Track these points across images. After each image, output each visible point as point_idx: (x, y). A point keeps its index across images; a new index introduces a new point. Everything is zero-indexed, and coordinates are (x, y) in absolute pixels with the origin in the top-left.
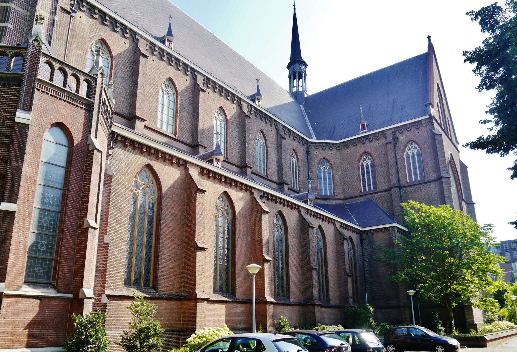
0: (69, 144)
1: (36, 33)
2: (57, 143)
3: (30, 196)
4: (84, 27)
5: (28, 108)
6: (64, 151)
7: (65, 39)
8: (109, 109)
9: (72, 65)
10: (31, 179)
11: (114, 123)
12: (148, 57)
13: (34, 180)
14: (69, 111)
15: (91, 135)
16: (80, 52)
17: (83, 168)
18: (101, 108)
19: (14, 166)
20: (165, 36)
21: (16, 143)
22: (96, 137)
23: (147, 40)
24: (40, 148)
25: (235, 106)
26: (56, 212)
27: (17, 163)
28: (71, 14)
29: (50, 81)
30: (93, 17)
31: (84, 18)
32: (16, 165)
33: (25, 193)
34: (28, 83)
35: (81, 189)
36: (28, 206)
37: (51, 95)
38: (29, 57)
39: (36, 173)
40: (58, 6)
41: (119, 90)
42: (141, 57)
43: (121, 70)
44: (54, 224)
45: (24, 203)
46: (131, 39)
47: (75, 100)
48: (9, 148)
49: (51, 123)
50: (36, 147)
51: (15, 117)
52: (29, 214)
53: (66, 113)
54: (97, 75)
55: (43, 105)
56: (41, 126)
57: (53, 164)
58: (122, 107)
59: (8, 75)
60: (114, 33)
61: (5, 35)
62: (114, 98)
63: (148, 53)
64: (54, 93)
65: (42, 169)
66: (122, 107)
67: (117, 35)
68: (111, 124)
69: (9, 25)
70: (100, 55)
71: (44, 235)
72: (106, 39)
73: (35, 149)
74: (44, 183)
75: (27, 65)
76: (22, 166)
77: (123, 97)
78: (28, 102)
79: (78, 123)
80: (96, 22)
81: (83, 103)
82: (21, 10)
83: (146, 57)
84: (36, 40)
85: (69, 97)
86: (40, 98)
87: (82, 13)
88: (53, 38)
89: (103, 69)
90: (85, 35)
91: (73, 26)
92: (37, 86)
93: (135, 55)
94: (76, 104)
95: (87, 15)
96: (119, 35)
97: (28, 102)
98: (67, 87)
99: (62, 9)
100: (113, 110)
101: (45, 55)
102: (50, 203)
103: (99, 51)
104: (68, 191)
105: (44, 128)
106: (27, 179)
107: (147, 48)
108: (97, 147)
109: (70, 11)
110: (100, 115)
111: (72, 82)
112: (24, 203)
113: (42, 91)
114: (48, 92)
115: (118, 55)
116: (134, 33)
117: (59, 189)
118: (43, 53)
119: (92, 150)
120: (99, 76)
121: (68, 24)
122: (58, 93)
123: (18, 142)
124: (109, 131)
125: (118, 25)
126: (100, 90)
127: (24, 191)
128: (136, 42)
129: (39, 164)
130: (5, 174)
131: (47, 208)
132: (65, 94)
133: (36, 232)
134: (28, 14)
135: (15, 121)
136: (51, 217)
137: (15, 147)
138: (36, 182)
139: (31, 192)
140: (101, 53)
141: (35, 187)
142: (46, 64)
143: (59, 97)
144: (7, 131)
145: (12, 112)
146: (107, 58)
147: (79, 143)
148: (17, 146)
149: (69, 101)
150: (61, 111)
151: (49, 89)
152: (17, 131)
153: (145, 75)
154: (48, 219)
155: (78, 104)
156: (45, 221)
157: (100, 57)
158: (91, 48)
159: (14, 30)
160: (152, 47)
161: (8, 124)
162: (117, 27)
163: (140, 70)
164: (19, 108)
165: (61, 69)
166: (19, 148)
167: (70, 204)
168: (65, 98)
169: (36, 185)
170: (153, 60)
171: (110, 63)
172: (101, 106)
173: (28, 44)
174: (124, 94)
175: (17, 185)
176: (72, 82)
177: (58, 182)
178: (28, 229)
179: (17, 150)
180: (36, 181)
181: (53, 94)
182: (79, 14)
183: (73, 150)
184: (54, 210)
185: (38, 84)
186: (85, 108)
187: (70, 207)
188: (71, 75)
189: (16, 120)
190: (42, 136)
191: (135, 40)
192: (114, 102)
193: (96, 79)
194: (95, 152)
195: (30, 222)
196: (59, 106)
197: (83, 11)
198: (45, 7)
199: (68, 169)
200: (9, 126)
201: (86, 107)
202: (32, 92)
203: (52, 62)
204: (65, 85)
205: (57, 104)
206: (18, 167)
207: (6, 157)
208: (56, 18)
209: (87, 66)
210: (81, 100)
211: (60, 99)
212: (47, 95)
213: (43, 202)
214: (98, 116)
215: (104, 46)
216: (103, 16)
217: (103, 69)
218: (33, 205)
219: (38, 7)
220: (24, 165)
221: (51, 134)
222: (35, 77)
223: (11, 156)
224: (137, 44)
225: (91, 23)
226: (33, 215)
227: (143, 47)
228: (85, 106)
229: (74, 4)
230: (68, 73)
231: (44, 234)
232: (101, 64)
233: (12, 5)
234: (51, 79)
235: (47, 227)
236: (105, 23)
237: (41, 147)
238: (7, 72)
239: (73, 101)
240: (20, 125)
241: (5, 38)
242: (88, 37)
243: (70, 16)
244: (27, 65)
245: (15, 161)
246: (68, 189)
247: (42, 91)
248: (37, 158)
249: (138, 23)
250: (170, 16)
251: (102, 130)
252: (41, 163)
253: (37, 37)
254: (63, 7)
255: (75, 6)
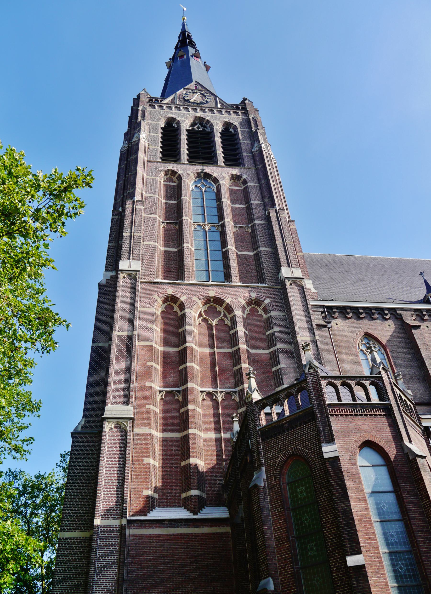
0: (386, 462)
1: (308, 361)
2: (373, 466)
3: (372, 540)
4: (344, 332)
5: (331, 440)
6: (383, 471)
7: (332, 352)
8: (409, 403)
9: (349, 374)
10: (365, 518)
11: (423, 417)
12: (420, 326)
13: (369, 518)
14: (371, 424)
15: (404, 441)
16: (351, 358)
17: (414, 485)
18: (400, 406)
19: (343, 509)
20: (426, 295)
21: (335, 482)
22: (410, 441)
23: (410, 310)
24: (359, 478)
25: (390, 322)
26: (407, 552)
27: (344, 504)
28: (328, 326)
29: (338, 401)
30: (348, 318)
31: (340, 323)
32: (344, 507)
33: (365, 538)
34: (321, 412)
35: (423, 512)
36: (375, 553)
37: (346, 415)
38: (311, 387)
39: (366, 509)
40: (314, 326)
41: (408, 377)
42: (413, 331)
43: (399, 355)
44: (413, 570)
45: (369, 551)
46: (394, 318)
47: (371, 409)
48: (330, 490)
49: (358, 445)
50: (355, 478)
51: (322, 453)
52: (380, 563)
53: (368, 428)
54: (380, 373)
55: (343, 430)
56: (351, 453)
57: (380, 492)
58: (420, 394)
59: (301, 414)
60: (374, 321)
61: (282, 377)
62: (408, 389)
63: (417, 322)
64: (347, 412)
65: (370, 501)
66: (420, 394)
67: (378, 321)
68: (419, 419)
69: (283, 366)
70: (373, 350)
71: (407, 588)
72: (370, 332)
73: (355, 482)
74: (380, 518)
75: (313, 395)
76: (350, 505)
77: (416, 382)
78: (328, 432)
79: (385, 433)
80: (353, 320)
81: (380, 409)
82: (286, 347)
83: (418, 327)
84: (311, 368)
85: (363, 409)
86: (338, 423)
87: (336, 320)
88: (322, 357)
89: (383, 363)
90: (348, 339)
91: (334, 336)
92: (330, 412)
93: (406, 332)
94: (373, 413)
95: (341, 319)
96: (380, 320)
97: (328, 432)
98: (357, 399)
99: (318, 326)
100: (413, 402)
101: (324, 378)
102: (396, 542)
103: (371, 347)
104: (410, 520)
105: (354, 454)
106: (360, 520)
107: (414, 317)
108: (418, 453)
109: (326, 324)
110: (404, 415)
111: (360, 393)
112: (369, 551)
113: (336, 415)
114: (341, 413)
115: (389, 341)
116: (393, 311)
117: (398, 520)
118: (321, 377)
119: (413, 459)
120: (383, 372)
121: (329, 337)
122: (351, 409)
123: (336, 480)
124: (421, 429)
125: (374, 311)
126: (390, 387)
127: (363, 536)
128: (399, 318)
129: (365, 497)
130: (337, 521)
131: (396, 550)
132: (358, 408)
133: (397, 585)
134: (293, 347)
135: (325, 457)
136: (405, 560)
137: (336, 487)
138: (371, 521)
139: (371, 535)
140: (373, 349)
141: (373, 527)
142: (327, 386)
143: (353, 413)
144: (321, 472)
145: (318, 450)
146: (379, 350)
147: (395, 456)
148: (337, 484)
149: (366, 413)
150: (362, 428)
151: (342, 409)
152: (330, 467)
153: (427, 347)
154: (403, 564)
155: (376, 413)
156: (401, 568)
157: (374, 352)
158: (359, 348)
159: (287, 368)
160: (419, 313)
161: (319, 464)
162: (374, 314)
163: (419, 345)
164: (322, 443)
165: (343, 384)
166: (339, 486)
167: (419, 537)
168: (359, 412)
169: (372, 524)
170: (427, 327)
171: (384, 353)
172: (399, 404)
173: (305, 375)
174: (415, 378)
175: (354, 530)
176: (360, 393)
177: (395, 512)
178: (386, 584)
179: (338, 489)
180: (370, 518)
181: (347, 414)
182: (334, 322)
183: (393, 467)
184: (405, 549)
185: (329, 409)
186: (384, 413)
187: (421, 541)
188: (355, 385)
189: (326, 456)
190: (355, 464)
191: (397, 317)
192: (411, 393)
193: (381, 378)
194: (418, 459)
195: (384, 574)
196: (358, 423)
197: (336, 318)
198: (304, 333)
199: (398, 492)
200: (321, 465)
201: (385, 412)
202: (328, 420)
203: (333, 381)
204: (354, 399)
205: (356, 422)
206: (347, 508)
207: (331, 501)
208: (317, 338)
209: (363, 368)
210: (376, 407)
211: (356, 415)
212: (342, 418)
213: (388, 544)
214: (402, 416)
215: (371, 339)
216: (356, 311)
217: (383, 363)
218: (378, 550)
219: (298, 336)
220: (351, 504)
221: (363, 458)
222: (324, 404)
223: (335, 498)
224: (402, 319)
225: (348, 324)
226: (384, 563)
227: (410, 319)
228: (383, 412)
229: (326, 316)
230: (352, 385)
231: (406, 586)
232: (378, 360)
233: (278, 347)
234: (339, 399)
235: (405, 575)
236: (361, 316)
237: (359, 476)
238: (298, 411)
239: (369, 412)
240: (330, 460)
241: (283, 379)
242: (352, 339)
243: (327, 329)
244: (313, 395)
245: (341, 502)
246: (409, 517)
247: (336, 415)
248: (361, 491)
249: (392, 299)
250: (421, 272)
251: (413, 430)
252: (367, 496)
253: (310, 365)
254: (318, 324)
255: (327, 317)
